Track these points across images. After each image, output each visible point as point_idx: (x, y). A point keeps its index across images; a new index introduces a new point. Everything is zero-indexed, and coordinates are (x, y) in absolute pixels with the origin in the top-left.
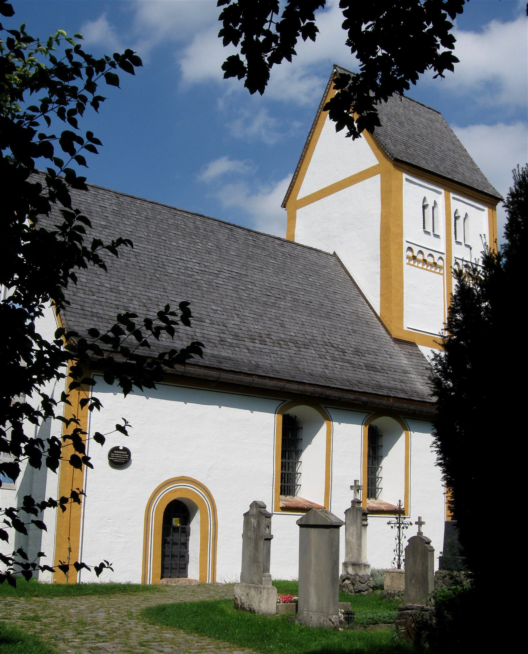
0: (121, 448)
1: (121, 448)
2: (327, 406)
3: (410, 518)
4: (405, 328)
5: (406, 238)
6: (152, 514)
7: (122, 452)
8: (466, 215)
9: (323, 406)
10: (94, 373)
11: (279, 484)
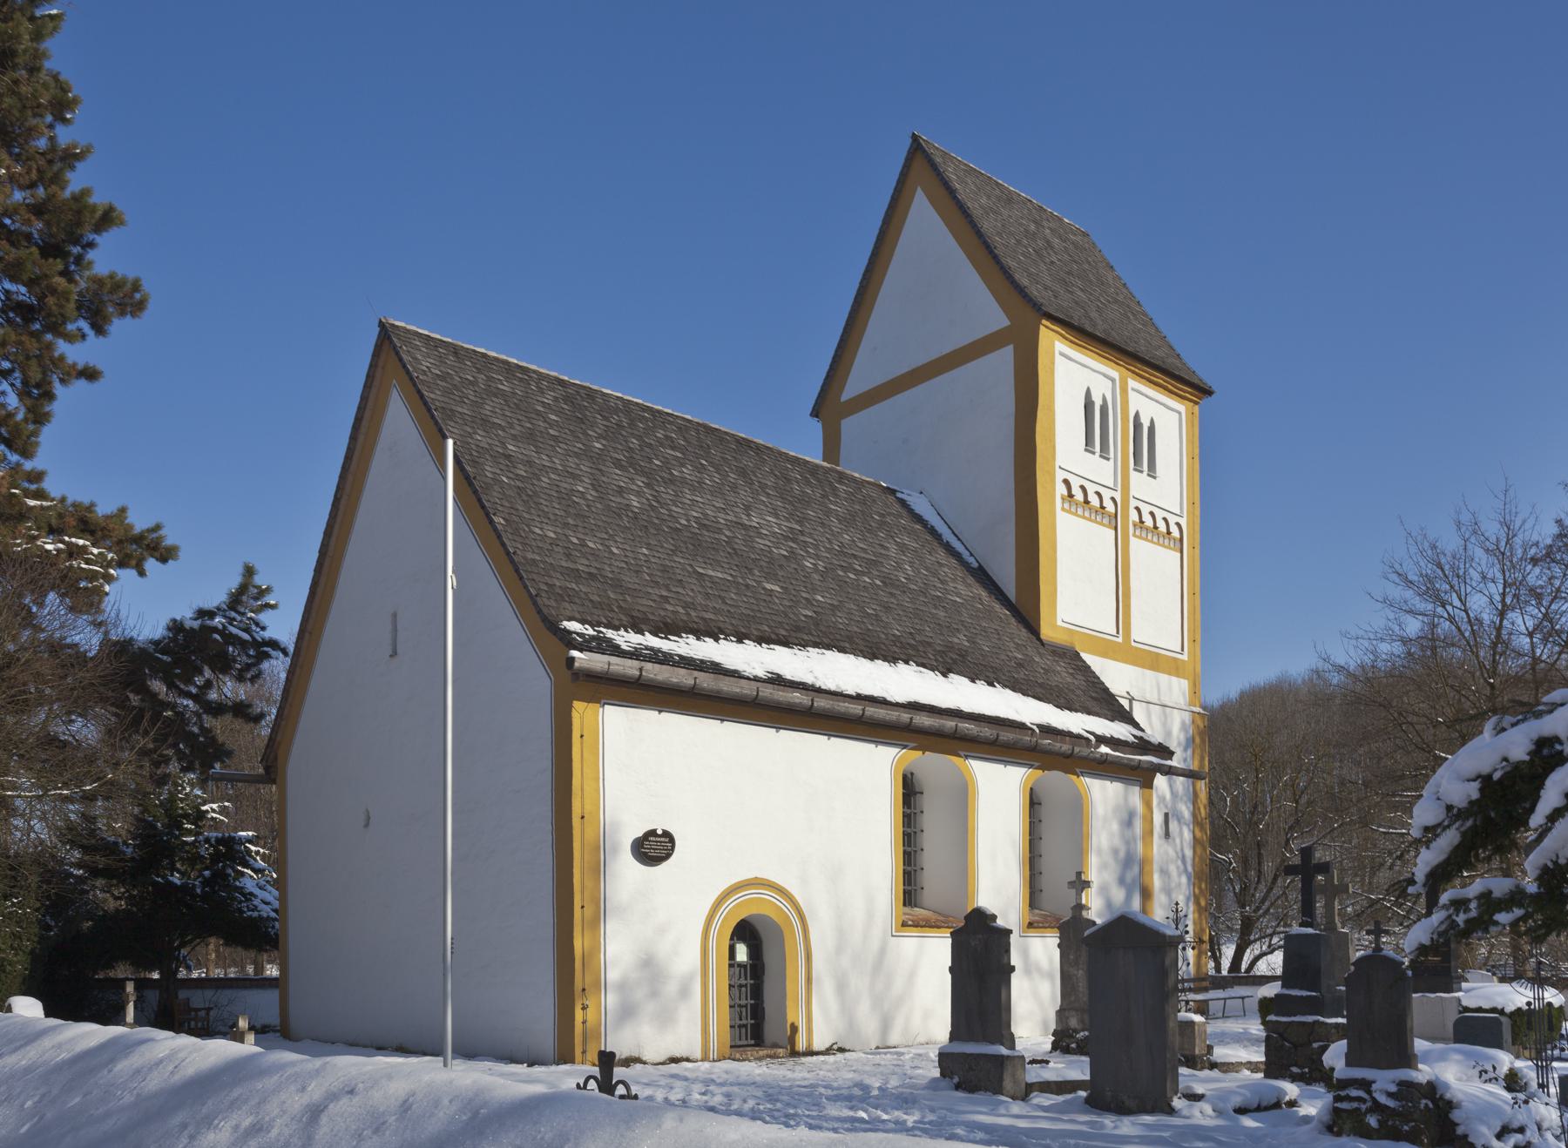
0: (660, 832)
1: (660, 832)
2: (969, 754)
3: (1020, 936)
4: (1059, 623)
5: (1058, 463)
6: (712, 943)
7: (662, 839)
8: (1152, 421)
10: (606, 701)
11: (901, 887)
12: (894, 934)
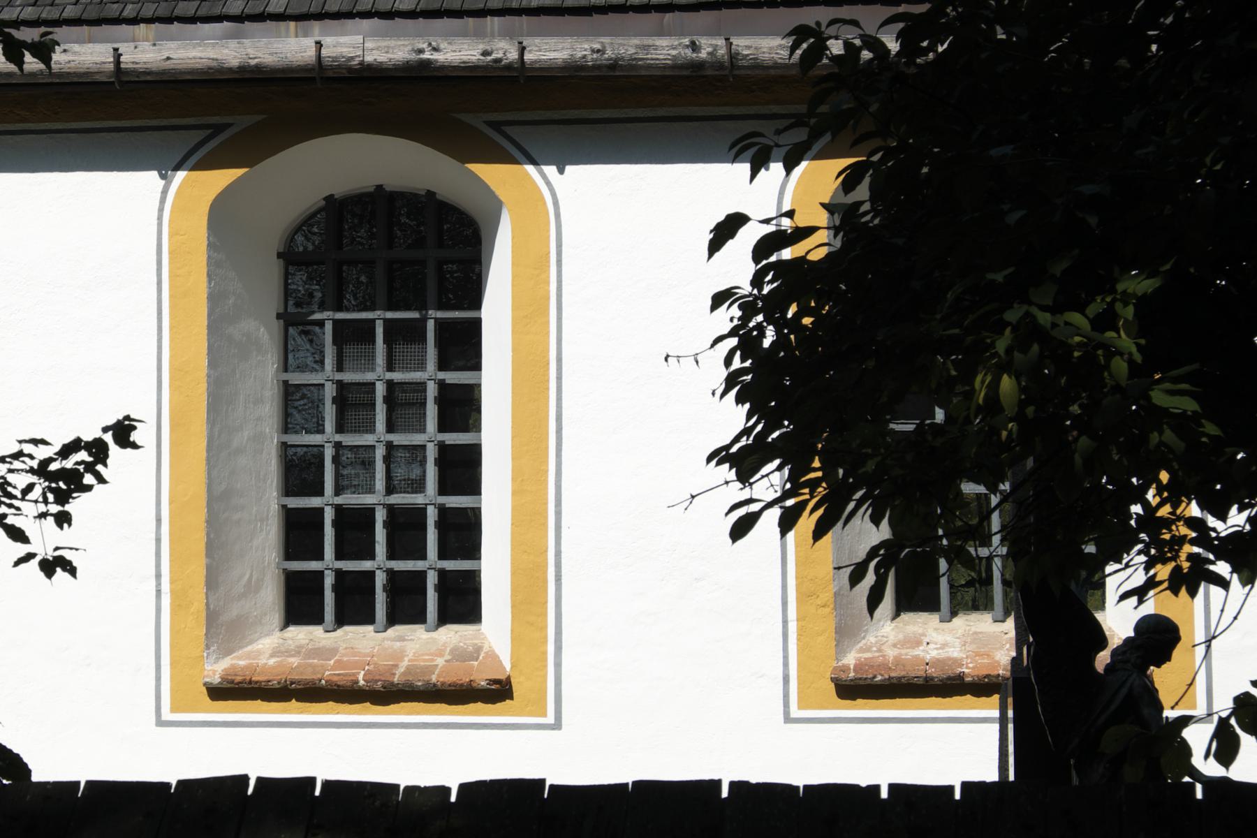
9: (477, 121)
12: (550, 719)
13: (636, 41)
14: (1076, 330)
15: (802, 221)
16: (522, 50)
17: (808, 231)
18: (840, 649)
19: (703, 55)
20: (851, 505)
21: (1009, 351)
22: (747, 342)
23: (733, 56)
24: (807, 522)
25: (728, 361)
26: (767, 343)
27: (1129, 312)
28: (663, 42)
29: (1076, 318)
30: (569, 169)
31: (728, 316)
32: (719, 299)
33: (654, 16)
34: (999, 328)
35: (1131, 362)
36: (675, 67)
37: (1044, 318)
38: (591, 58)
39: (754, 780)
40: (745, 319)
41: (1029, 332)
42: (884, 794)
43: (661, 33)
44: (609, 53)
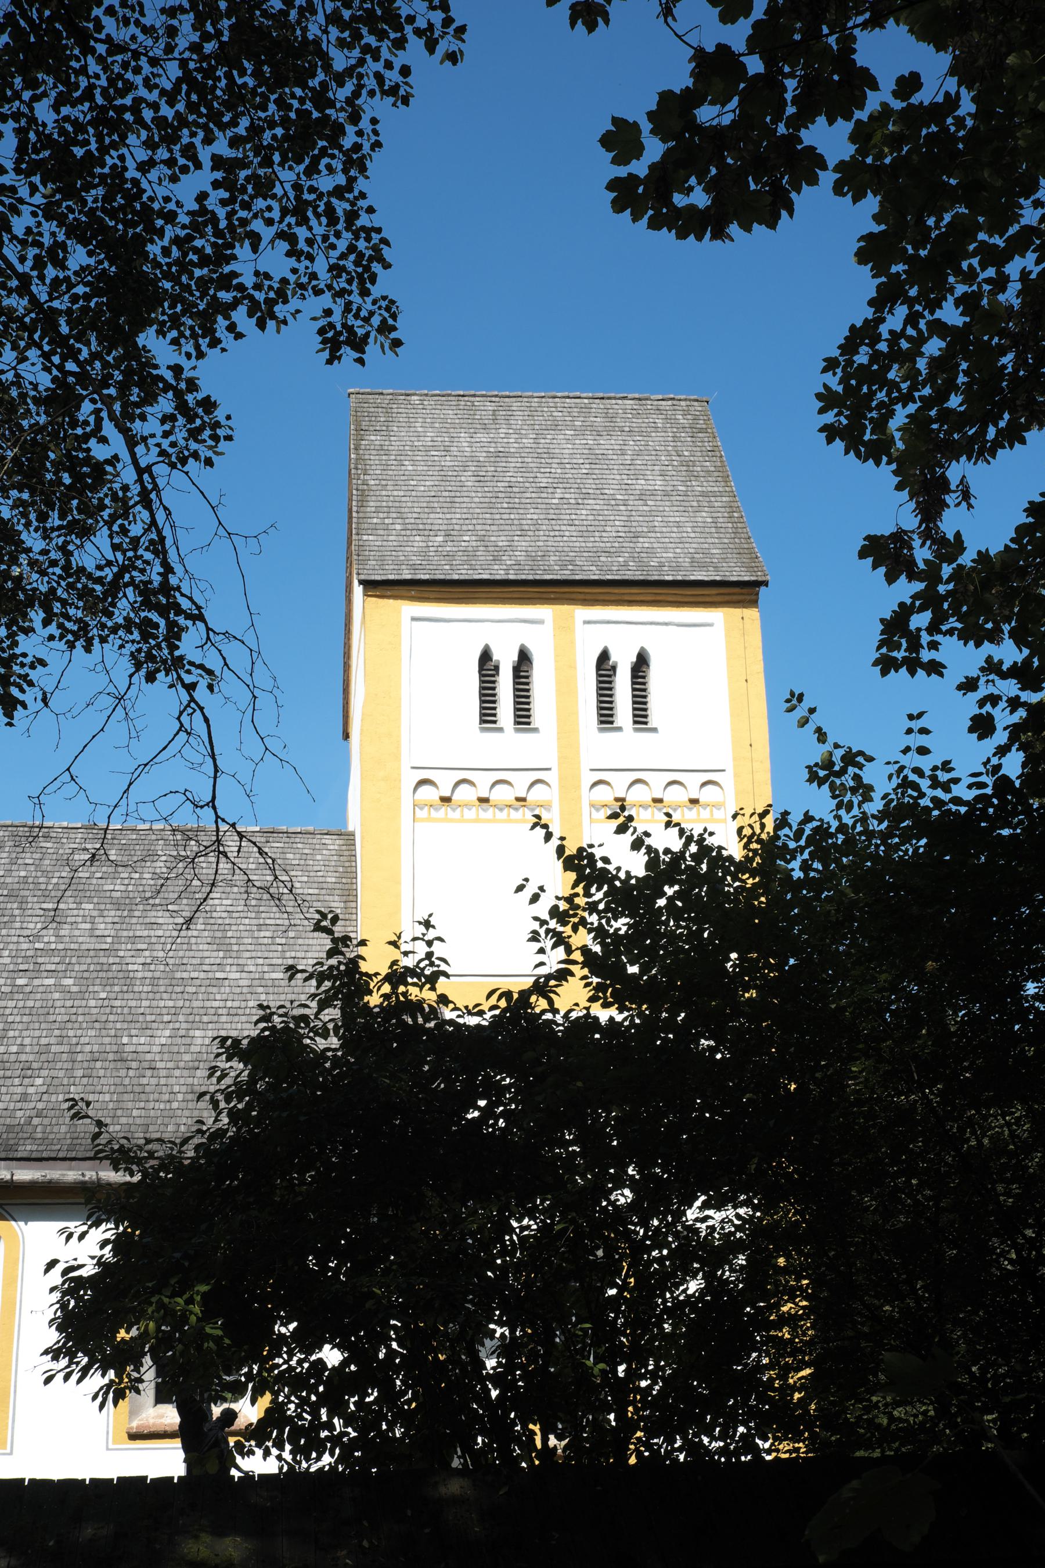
3: (11, 1453)
12: (8, 1451)
13: (60, 1172)
14: (178, 1304)
15: (80, 1262)
16: (12, 1175)
17: (82, 1266)
18: (130, 1420)
19: (87, 1178)
20: (92, 1371)
21: (153, 1312)
22: (63, 1306)
23: (99, 1179)
24: (75, 1377)
25: (55, 1313)
26: (71, 1307)
27: (198, 1298)
28: (71, 1173)
29: (179, 1300)
30: (30, 1223)
31: (56, 1296)
32: (52, 1290)
33: (68, 1162)
34: (151, 1304)
35: (198, 1318)
36: (75, 1183)
37: (166, 1300)
38: (41, 1179)
39: (38, 1478)
40: (62, 1297)
41: (161, 1305)
42: (176, 1481)
43: (70, 1169)
44: (48, 1177)
